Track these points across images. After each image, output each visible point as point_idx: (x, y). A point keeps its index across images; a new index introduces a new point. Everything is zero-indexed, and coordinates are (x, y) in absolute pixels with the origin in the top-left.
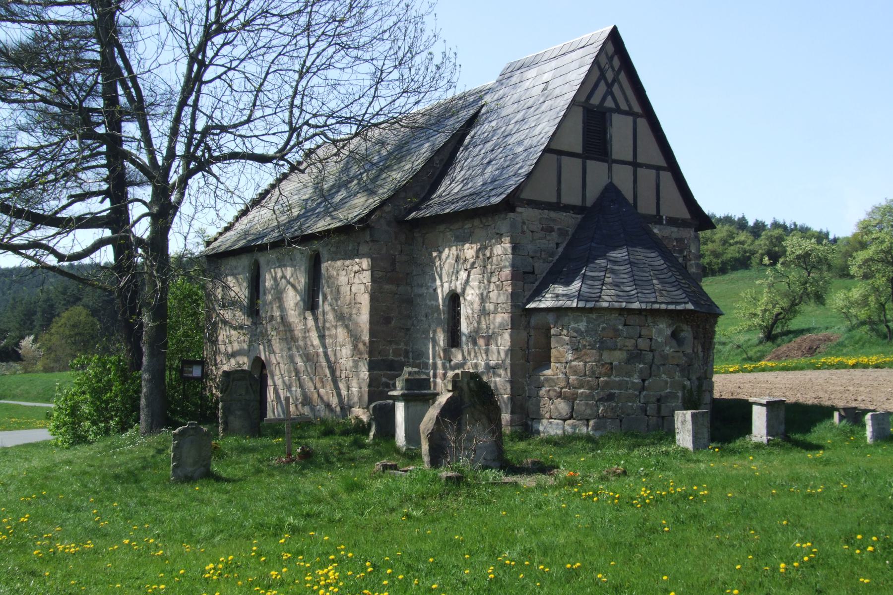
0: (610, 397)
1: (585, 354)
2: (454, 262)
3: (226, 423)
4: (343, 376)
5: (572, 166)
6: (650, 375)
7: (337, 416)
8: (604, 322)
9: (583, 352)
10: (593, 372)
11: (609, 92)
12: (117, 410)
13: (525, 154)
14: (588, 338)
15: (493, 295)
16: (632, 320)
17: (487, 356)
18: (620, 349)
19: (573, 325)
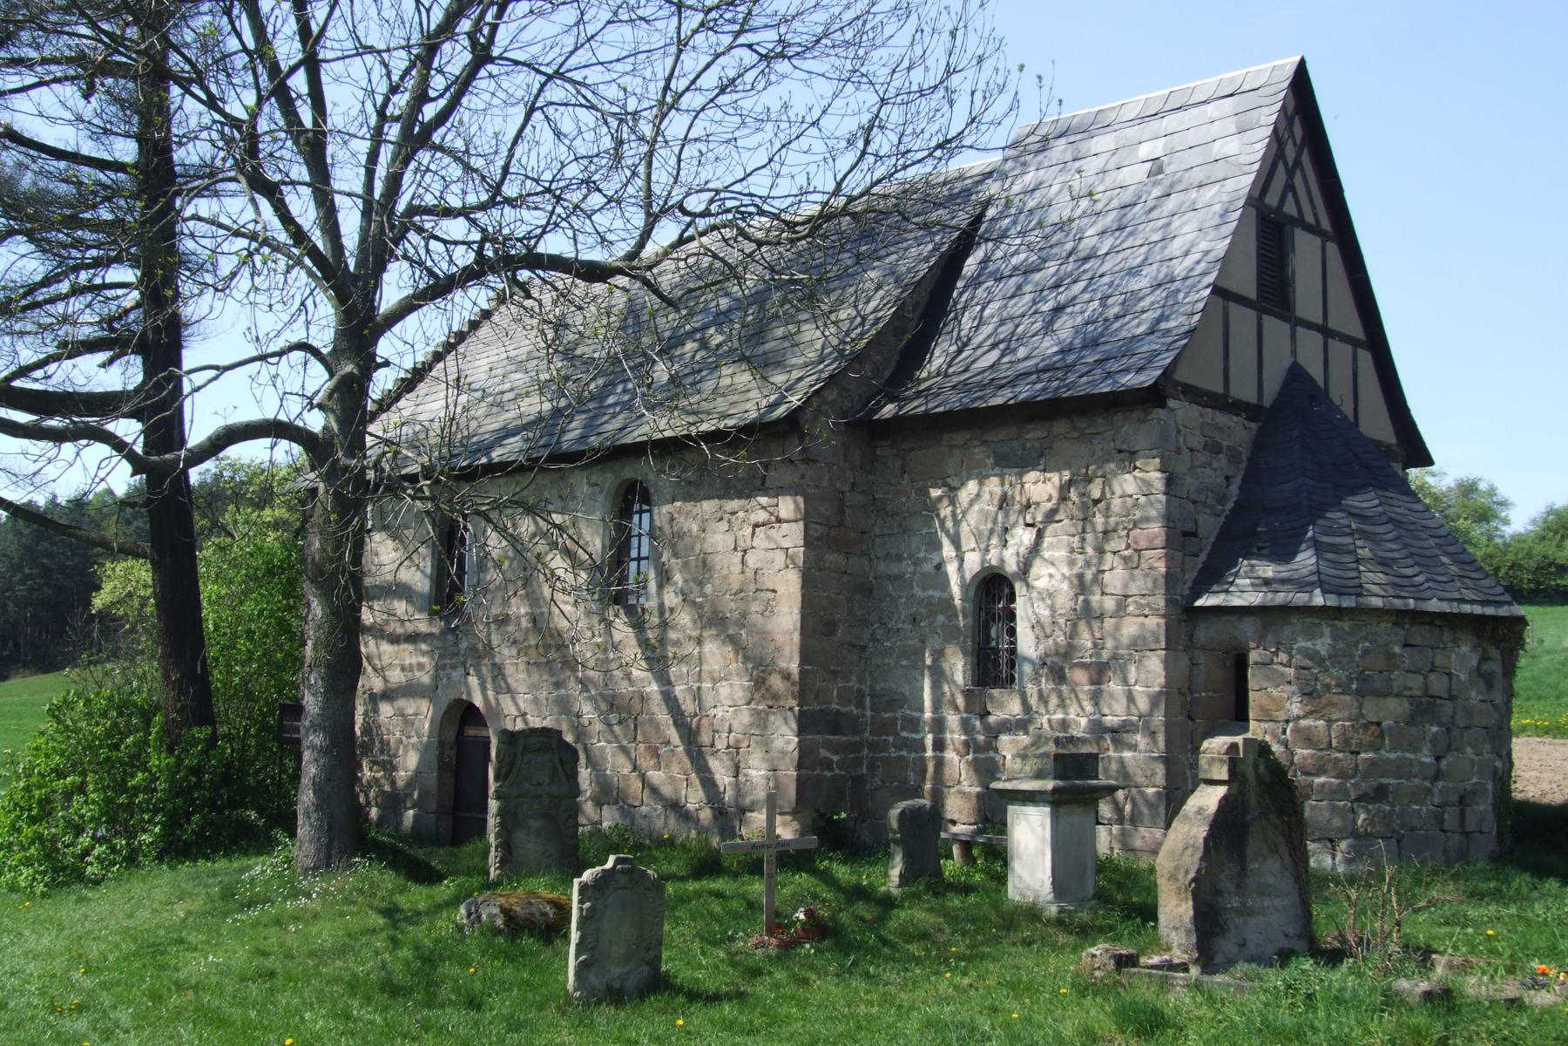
0: (1380, 793)
1: (1330, 704)
2: (993, 509)
3: (506, 846)
4: (721, 744)
5: (1244, 320)
6: (1449, 748)
7: (701, 830)
8: (1365, 639)
9: (1324, 701)
10: (1346, 744)
11: (1289, 187)
12: (156, 812)
13: (1160, 294)
14: (1333, 671)
15: (1115, 577)
16: (1420, 634)
17: (1096, 704)
18: (1398, 695)
19: (1301, 643)
